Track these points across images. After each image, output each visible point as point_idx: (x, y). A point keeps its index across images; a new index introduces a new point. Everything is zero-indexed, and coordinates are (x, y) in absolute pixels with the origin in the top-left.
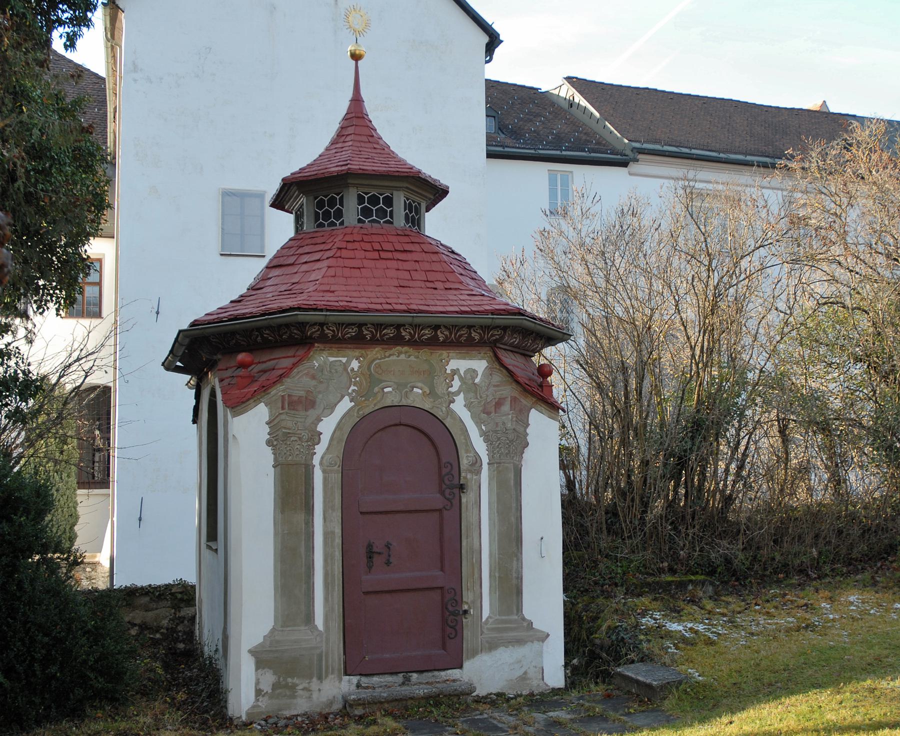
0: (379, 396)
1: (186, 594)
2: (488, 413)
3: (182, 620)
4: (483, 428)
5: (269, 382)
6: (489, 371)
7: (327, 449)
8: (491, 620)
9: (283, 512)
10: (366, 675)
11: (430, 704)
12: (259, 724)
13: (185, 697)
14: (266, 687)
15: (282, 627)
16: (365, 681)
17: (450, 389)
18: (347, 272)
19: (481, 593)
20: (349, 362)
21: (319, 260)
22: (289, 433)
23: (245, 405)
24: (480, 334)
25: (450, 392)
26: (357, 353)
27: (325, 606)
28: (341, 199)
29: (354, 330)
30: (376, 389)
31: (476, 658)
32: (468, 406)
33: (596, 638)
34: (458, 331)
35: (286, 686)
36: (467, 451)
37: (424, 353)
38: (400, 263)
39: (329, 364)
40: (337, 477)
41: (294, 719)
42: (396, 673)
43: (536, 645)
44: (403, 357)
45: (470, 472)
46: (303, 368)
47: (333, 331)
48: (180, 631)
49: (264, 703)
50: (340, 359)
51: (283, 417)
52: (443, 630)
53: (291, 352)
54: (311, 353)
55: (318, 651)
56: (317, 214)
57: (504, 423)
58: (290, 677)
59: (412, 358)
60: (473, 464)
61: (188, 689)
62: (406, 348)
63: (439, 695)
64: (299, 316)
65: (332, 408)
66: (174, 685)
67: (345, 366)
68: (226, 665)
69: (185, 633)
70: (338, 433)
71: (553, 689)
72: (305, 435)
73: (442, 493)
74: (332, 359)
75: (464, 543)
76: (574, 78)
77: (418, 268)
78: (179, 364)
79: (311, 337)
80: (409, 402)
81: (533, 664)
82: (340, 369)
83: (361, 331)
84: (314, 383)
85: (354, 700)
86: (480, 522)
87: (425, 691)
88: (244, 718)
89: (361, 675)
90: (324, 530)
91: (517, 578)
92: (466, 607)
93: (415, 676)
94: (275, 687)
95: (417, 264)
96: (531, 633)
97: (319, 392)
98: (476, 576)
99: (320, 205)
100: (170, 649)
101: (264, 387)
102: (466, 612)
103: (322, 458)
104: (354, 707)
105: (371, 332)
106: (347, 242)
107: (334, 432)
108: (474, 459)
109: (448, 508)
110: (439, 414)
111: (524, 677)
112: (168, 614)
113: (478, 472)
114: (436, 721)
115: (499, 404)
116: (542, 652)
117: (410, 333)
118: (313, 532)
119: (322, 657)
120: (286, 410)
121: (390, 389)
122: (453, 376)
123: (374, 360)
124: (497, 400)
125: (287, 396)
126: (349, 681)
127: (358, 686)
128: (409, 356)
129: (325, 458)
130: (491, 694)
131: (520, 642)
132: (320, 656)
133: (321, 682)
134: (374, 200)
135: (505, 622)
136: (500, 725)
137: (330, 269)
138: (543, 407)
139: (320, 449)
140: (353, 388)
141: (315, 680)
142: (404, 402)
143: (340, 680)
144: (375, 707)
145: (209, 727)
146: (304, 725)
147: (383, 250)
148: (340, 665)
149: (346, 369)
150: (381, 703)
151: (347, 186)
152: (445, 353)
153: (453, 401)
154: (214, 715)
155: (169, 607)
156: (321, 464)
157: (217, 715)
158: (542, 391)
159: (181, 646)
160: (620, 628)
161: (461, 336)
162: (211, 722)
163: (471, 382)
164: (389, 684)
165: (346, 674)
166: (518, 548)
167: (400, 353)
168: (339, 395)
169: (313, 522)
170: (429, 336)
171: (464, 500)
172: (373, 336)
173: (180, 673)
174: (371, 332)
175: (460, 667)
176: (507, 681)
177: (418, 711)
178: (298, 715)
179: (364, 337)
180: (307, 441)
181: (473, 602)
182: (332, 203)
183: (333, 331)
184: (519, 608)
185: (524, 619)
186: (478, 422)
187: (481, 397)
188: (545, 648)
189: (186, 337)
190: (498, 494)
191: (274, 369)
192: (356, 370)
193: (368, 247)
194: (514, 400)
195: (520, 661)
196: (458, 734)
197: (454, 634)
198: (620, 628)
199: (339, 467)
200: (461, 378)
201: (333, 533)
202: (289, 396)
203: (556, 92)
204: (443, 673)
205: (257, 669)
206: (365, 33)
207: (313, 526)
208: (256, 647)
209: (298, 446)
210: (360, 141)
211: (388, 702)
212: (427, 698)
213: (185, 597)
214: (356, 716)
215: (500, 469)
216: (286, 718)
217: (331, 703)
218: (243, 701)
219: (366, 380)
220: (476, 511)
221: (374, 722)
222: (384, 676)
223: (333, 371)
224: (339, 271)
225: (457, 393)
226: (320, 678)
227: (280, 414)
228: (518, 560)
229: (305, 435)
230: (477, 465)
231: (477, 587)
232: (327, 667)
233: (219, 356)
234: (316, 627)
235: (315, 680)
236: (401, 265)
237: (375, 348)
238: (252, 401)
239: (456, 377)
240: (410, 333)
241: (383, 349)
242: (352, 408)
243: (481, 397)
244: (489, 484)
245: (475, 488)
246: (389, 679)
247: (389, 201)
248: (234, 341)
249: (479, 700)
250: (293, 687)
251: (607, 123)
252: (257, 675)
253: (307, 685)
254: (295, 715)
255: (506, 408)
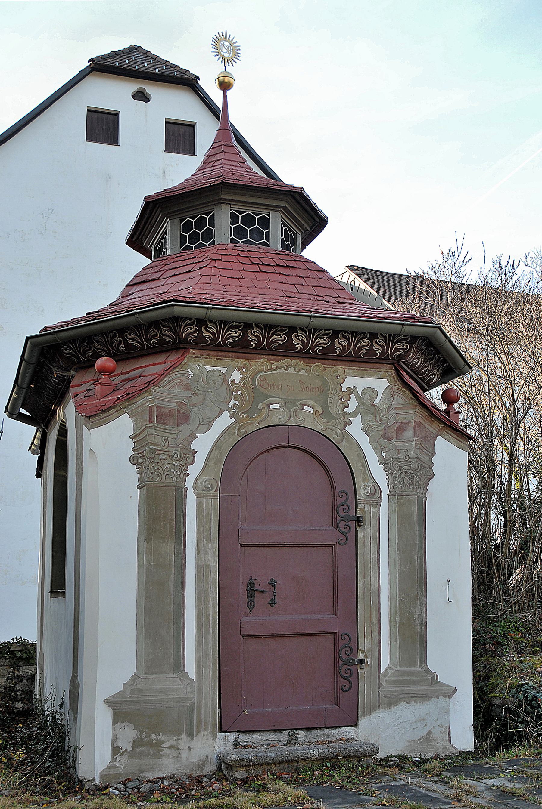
0: (264, 413)
1: (26, 653)
2: (389, 439)
3: (20, 679)
4: (383, 454)
5: (135, 389)
6: (390, 392)
7: (203, 470)
8: (390, 672)
9: (148, 540)
10: (244, 732)
11: (326, 766)
12: (116, 789)
13: (23, 756)
14: (126, 744)
15: (146, 673)
16: (243, 738)
17: (346, 410)
18: (226, 281)
19: (380, 640)
20: (229, 373)
21: (190, 271)
22: (157, 450)
23: (106, 415)
24: (382, 347)
25: (346, 413)
26: (239, 363)
27: (197, 651)
28: (212, 219)
29: (238, 334)
30: (261, 405)
31: (373, 715)
32: (366, 429)
33: (494, 697)
34: (358, 342)
35: (150, 743)
36: (365, 480)
37: (317, 367)
38: (284, 277)
39: (206, 373)
40: (213, 503)
41: (160, 783)
42: (280, 731)
43: (442, 701)
44: (292, 370)
45: (368, 503)
46: (175, 376)
47: (213, 334)
48: (18, 691)
49: (122, 763)
50: (219, 369)
51: (151, 431)
52: (336, 683)
53: (161, 358)
54: (185, 360)
55: (189, 703)
56: (183, 238)
57: (406, 451)
58: (154, 733)
59: (303, 372)
60: (371, 495)
61: (27, 748)
62: (295, 361)
63: (337, 756)
64: (175, 307)
65: (209, 424)
66: (10, 744)
67: (225, 377)
68: (75, 719)
69: (23, 692)
70: (215, 453)
71: (461, 752)
72: (177, 453)
73: (336, 525)
74: (209, 368)
75: (360, 584)
76: (355, 266)
77: (304, 283)
78: (22, 411)
79: (185, 341)
80: (299, 421)
81: (439, 723)
82: (219, 380)
83: (245, 335)
84: (188, 394)
85: (235, 761)
86: (379, 560)
87: (321, 751)
88: (97, 781)
89: (239, 731)
90: (197, 563)
91: (421, 625)
92: (361, 656)
93: (302, 733)
94: (136, 744)
95: (302, 279)
96: (436, 687)
97: (194, 405)
98: (374, 621)
99: (187, 227)
100: (7, 707)
101: (128, 394)
102: (361, 661)
103: (196, 480)
104: (235, 770)
105: (257, 337)
106: (222, 255)
107: (211, 451)
108: (373, 488)
109: (342, 542)
110: (334, 437)
111: (428, 738)
112: (6, 673)
113: (378, 504)
114: (342, 787)
115: (401, 429)
116: (448, 710)
117: (302, 341)
118: (184, 565)
119: (193, 710)
120: (155, 423)
121: (277, 406)
122: (350, 395)
123: (259, 372)
124: (399, 424)
125: (155, 409)
126: (225, 738)
127: (236, 744)
128: (300, 370)
129: (200, 480)
130: (391, 756)
131: (424, 697)
132: (191, 709)
133: (192, 739)
134: (249, 220)
135: (408, 674)
136: (434, 795)
137: (203, 277)
138: (451, 435)
139: (194, 470)
140: (233, 402)
141: (184, 736)
142: (293, 422)
143: (215, 737)
144: (260, 770)
145: (54, 791)
146: (173, 790)
147: (263, 264)
148: (215, 720)
149: (225, 381)
150: (268, 764)
151: (219, 202)
152: (340, 369)
153: (350, 423)
154: (58, 777)
155: (7, 665)
156: (195, 487)
157: (63, 777)
158: (449, 417)
159: (19, 705)
160: (526, 687)
161: (360, 348)
162: (56, 785)
163: (369, 403)
164: (272, 743)
165: (221, 730)
166: (422, 591)
167: (288, 367)
168: (218, 410)
169: (184, 553)
170: (324, 346)
171: (360, 535)
172: (260, 343)
173: (18, 731)
174: (257, 337)
175: (355, 725)
176: (409, 741)
177: (313, 775)
178: (164, 778)
179: (248, 343)
180: (179, 461)
181: (371, 650)
182: (200, 223)
183: (213, 334)
184: (423, 659)
185: (428, 671)
186: (378, 448)
187: (381, 420)
188: (451, 705)
189: (34, 345)
190: (399, 531)
191: (140, 377)
192: (237, 382)
193: (246, 261)
194: (418, 425)
195: (424, 720)
196: (384, 805)
197: (348, 686)
198: (526, 687)
199: (216, 491)
200: (358, 398)
201: (208, 566)
202: (158, 407)
203: (339, 279)
204: (334, 731)
205: (114, 723)
206: (234, 63)
207: (184, 558)
208: (113, 697)
209: (168, 466)
210: (231, 165)
211: (276, 763)
212: (323, 759)
213: (25, 656)
214: (237, 779)
215: (402, 501)
216: (150, 781)
217: (203, 764)
218: (97, 760)
219: (249, 394)
220: (374, 548)
221: (263, 787)
222: (266, 733)
223: (211, 382)
224: (215, 279)
225: (354, 414)
226: (190, 735)
227: (148, 427)
228: (421, 604)
229: (177, 453)
230: (376, 496)
231: (375, 634)
232: (199, 722)
233: (73, 372)
234: (186, 675)
235: (184, 736)
236: (283, 279)
237: (260, 359)
238: (114, 410)
239: (353, 396)
240: (302, 341)
241: (269, 360)
242: (232, 424)
243: (381, 420)
244: (390, 518)
245: (374, 521)
246: (272, 736)
247: (265, 222)
248: (91, 352)
249: (385, 762)
250: (158, 745)
251: (384, 301)
252: (114, 729)
253: (175, 743)
254: (160, 778)
255: (409, 433)
